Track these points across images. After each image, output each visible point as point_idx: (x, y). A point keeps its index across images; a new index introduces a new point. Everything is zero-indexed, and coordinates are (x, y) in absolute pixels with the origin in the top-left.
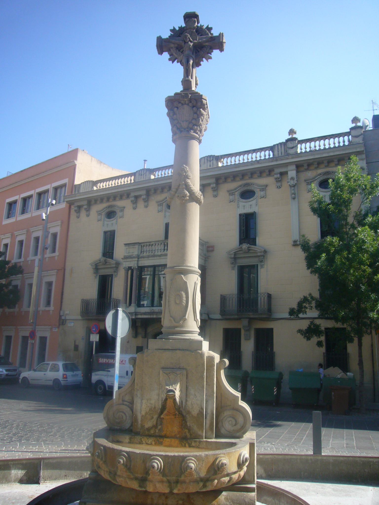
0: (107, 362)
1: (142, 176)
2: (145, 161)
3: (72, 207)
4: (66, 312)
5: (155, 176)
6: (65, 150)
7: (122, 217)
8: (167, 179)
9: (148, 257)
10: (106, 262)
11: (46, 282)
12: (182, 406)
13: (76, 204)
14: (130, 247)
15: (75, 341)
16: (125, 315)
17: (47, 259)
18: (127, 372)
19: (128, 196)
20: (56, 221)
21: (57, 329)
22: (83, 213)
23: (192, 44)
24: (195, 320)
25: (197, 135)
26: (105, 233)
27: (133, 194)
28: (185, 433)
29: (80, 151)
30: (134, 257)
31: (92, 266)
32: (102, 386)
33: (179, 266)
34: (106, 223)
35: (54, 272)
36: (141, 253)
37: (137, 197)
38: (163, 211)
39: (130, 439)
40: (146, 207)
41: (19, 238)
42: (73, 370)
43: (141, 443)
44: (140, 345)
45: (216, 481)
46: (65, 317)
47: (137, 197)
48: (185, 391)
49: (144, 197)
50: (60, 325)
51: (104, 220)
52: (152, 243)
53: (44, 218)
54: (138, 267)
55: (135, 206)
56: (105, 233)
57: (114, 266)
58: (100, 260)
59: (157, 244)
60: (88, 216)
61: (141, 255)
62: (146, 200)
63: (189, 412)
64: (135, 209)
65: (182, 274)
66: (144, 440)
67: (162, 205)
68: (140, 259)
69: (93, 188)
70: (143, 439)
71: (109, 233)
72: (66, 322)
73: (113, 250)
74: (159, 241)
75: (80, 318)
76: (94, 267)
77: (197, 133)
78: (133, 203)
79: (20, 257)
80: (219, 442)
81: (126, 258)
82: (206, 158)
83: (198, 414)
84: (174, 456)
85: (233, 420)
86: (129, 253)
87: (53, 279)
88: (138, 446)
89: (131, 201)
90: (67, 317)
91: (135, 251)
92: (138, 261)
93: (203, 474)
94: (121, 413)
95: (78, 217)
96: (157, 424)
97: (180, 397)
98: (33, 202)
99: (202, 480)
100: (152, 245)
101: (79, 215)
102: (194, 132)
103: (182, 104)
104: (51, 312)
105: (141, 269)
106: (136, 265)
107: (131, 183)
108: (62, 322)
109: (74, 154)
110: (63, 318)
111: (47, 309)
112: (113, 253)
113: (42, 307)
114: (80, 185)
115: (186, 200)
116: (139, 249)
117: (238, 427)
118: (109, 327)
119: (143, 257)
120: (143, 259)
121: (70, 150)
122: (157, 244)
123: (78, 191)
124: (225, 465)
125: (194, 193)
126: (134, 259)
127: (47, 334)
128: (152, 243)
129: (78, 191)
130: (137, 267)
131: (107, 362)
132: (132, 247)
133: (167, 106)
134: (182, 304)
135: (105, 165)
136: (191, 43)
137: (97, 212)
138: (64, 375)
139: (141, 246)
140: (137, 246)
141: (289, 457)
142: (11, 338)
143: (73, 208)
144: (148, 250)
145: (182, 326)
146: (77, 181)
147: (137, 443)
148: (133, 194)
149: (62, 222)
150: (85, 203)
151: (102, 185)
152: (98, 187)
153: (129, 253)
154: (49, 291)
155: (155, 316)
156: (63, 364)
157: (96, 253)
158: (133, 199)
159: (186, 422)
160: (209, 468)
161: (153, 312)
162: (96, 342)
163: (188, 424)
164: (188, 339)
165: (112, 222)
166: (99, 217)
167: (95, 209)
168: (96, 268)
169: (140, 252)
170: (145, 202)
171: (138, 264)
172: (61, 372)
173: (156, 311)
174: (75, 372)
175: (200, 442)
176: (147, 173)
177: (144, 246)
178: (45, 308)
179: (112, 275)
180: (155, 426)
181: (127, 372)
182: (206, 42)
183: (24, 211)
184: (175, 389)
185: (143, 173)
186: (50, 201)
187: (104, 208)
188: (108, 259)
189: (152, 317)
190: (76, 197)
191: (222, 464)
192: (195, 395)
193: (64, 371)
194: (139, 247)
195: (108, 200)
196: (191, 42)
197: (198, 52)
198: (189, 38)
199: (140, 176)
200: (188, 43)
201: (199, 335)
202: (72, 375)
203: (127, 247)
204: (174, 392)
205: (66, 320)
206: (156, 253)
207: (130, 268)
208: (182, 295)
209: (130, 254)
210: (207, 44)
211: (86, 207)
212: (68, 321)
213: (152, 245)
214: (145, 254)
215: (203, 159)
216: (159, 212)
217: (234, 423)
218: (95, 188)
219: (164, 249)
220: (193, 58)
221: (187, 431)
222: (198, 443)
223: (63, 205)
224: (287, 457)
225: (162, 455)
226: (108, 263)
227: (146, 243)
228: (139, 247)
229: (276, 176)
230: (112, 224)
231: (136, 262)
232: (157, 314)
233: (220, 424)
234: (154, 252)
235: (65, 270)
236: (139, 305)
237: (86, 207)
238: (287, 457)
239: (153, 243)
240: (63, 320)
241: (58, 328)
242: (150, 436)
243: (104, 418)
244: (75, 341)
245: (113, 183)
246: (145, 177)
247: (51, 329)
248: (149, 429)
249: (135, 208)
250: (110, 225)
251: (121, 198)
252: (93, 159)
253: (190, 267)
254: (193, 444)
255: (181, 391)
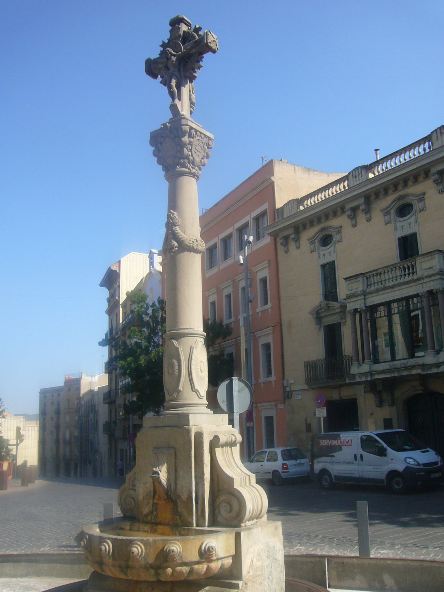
0: (330, 444)
1: (357, 178)
2: (376, 150)
3: (278, 240)
4: (292, 381)
5: (374, 174)
6: (258, 166)
7: (340, 241)
8: (387, 176)
9: (377, 291)
10: (328, 307)
11: (262, 345)
12: (171, 489)
13: (282, 235)
14: (352, 281)
15: (306, 419)
16: (243, 385)
17: (260, 314)
18: (355, 456)
19: (343, 211)
20: (261, 262)
21: (283, 405)
22: (292, 245)
23: (174, 59)
24: (192, 391)
25: (187, 170)
26: (323, 266)
27: (348, 206)
28: (177, 520)
29: (276, 162)
30: (359, 295)
31: (312, 314)
32: (328, 478)
33: (172, 330)
34: (322, 253)
35: (270, 330)
36: (367, 287)
37: (354, 210)
38: (392, 222)
39: (131, 525)
40: (369, 220)
41: (225, 292)
42: (295, 458)
43: (138, 530)
44: (388, 417)
45: (169, 570)
46: (290, 388)
47: (354, 210)
48: (173, 472)
49: (363, 207)
50: (285, 399)
51: (318, 249)
52: (379, 271)
53: (242, 262)
54: (367, 307)
55: (354, 222)
56: (323, 266)
57: (339, 310)
58: (320, 306)
59: (386, 271)
60: (298, 247)
61: (368, 290)
62: (368, 211)
63: (179, 497)
64: (355, 226)
65: (174, 339)
66: (142, 526)
67: (390, 213)
68: (367, 297)
69: (298, 208)
70: (140, 526)
71: (328, 266)
72: (291, 394)
73: (336, 288)
74: (387, 266)
75: (306, 387)
76: (315, 316)
77: (186, 167)
78: (351, 219)
79: (230, 317)
80: (199, 530)
81: (349, 297)
82: (438, 131)
83: (187, 498)
84: (122, 539)
85: (228, 507)
86: (351, 290)
87: (270, 339)
88: (136, 533)
89: (348, 217)
90: (293, 388)
91: (359, 286)
92: (365, 299)
93: (151, 560)
94: (131, 499)
95: (287, 252)
96: (152, 509)
97: (168, 480)
98: (234, 243)
99: (152, 567)
100: (381, 273)
101: (288, 249)
102: (181, 167)
103: (165, 138)
104: (273, 383)
105: (373, 309)
106: (363, 306)
107: (345, 190)
108: (287, 395)
109: (268, 169)
110: (288, 389)
111: (269, 379)
112: (336, 292)
113: (262, 379)
114: (282, 208)
115: (176, 251)
116: (364, 282)
117: (234, 513)
118: (224, 401)
119: (371, 293)
120: (370, 295)
121: (265, 163)
122: (386, 271)
123: (282, 217)
124: (173, 552)
125: (183, 241)
126: (359, 298)
127: (272, 413)
128: (379, 271)
129: (282, 217)
130: (364, 308)
131: (330, 444)
132: (354, 280)
133: (152, 144)
134: (174, 374)
135: (315, 172)
136: (181, 57)
137: (308, 240)
138: (283, 464)
139: (367, 278)
140: (360, 279)
141: (429, 564)
142: (273, 419)
143: (279, 241)
144: (376, 281)
145: (176, 399)
146: (279, 204)
147: (136, 531)
148: (348, 206)
149: (269, 263)
150: (291, 231)
151: (310, 202)
152: (306, 206)
153: (351, 290)
154: (269, 356)
155: (396, 374)
156: (282, 451)
157: (315, 296)
158: (436, 176)
159: (177, 508)
160: (158, 555)
161: (395, 368)
162: (324, 418)
163: (179, 509)
164: (180, 414)
165: (328, 250)
166: (312, 246)
167: (307, 235)
168: (318, 316)
169: (366, 287)
170: (366, 213)
171: (365, 303)
172: (280, 461)
173: (397, 367)
174: (299, 461)
175: (189, 530)
176: (363, 172)
177: (370, 277)
178: (265, 379)
179: (340, 323)
180: (151, 512)
181: (355, 456)
182: (192, 48)
183: (226, 256)
184: (160, 471)
185: (357, 174)
186: (246, 238)
187: (317, 233)
188: (330, 302)
189: (393, 376)
190: (278, 225)
191: (169, 550)
192: (184, 477)
193: (284, 460)
194: (364, 280)
195: (319, 221)
196: (174, 55)
197: (187, 62)
198: (171, 53)
199: (355, 179)
200: (170, 58)
201: (207, 407)
202: (295, 465)
203: (348, 282)
204: (158, 474)
205: (291, 392)
206: (387, 284)
207: (356, 311)
208: (174, 363)
209: (353, 291)
210: (194, 51)
211: (293, 236)
212: (294, 393)
213: (381, 273)
214: (372, 288)
215: (435, 132)
216: (386, 224)
217: (229, 509)
218: (302, 208)
219: (405, 275)
220: (177, 77)
221: (178, 517)
222: (187, 531)
223: (267, 240)
224: (425, 564)
225: (112, 538)
226: (331, 308)
227: (372, 271)
228: (364, 280)
229: (433, 178)
230: (330, 253)
231: (362, 301)
232: (398, 371)
233: (217, 511)
234: (383, 282)
235: (281, 325)
236: (376, 361)
237: (293, 236)
238: (425, 564)
239: (381, 270)
240: (288, 392)
241: (284, 403)
242: (147, 523)
243: (118, 504)
244: (306, 419)
245: (321, 197)
246: (360, 178)
247: (276, 405)
248: (146, 516)
249: (354, 226)
250: (327, 255)
251: (335, 214)
252: (297, 168)
253: (184, 329)
254: (183, 532)
255: (168, 472)
